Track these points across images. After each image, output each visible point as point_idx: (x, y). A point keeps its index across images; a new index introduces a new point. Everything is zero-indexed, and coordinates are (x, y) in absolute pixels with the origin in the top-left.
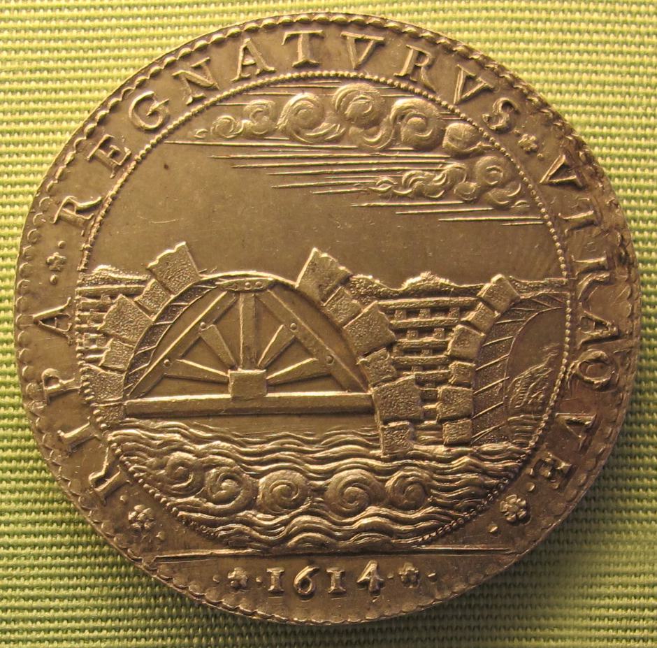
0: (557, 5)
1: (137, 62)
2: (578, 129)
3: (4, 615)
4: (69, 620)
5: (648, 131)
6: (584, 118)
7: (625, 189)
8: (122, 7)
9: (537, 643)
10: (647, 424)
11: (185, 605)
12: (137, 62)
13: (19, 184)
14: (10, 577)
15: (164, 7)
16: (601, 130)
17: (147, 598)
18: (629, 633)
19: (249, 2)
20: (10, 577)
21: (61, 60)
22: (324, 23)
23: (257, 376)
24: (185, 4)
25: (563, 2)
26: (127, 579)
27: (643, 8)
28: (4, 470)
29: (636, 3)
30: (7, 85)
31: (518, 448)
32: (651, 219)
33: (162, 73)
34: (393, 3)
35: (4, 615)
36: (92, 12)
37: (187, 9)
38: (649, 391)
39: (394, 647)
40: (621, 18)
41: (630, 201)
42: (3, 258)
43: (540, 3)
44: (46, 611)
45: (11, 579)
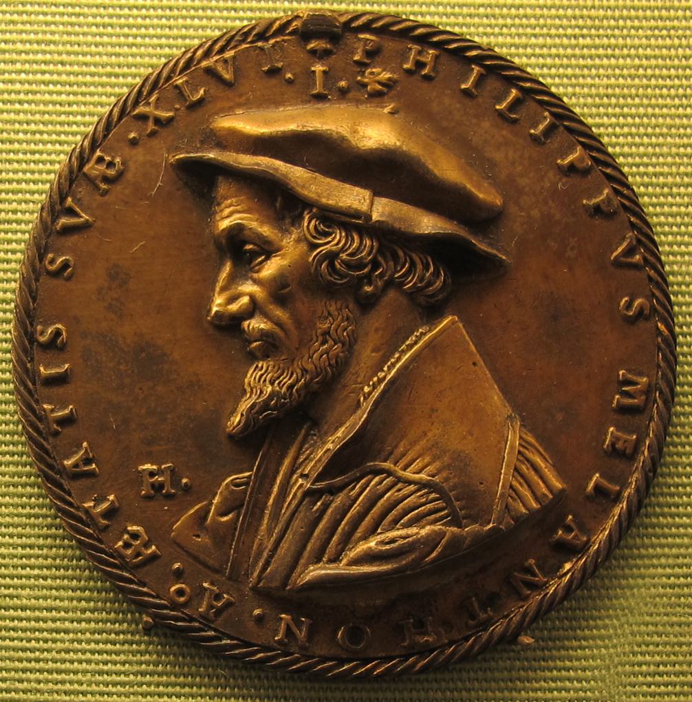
3: (3, 418)
5: (685, 121)
7: (650, 196)
8: (113, 7)
9: (9, 695)
10: (683, 446)
12: (229, 23)
16: (508, 51)
17: (158, 655)
21: (73, 73)
22: (384, 31)
23: (386, 573)
24: (36, 3)
25: (292, 2)
29: (409, 3)
30: (7, 76)
35: (3, 418)
37: (61, 9)
38: (684, 414)
41: (655, 208)
42: (5, 291)
43: (245, 2)
44: (53, 642)
45: (16, 548)
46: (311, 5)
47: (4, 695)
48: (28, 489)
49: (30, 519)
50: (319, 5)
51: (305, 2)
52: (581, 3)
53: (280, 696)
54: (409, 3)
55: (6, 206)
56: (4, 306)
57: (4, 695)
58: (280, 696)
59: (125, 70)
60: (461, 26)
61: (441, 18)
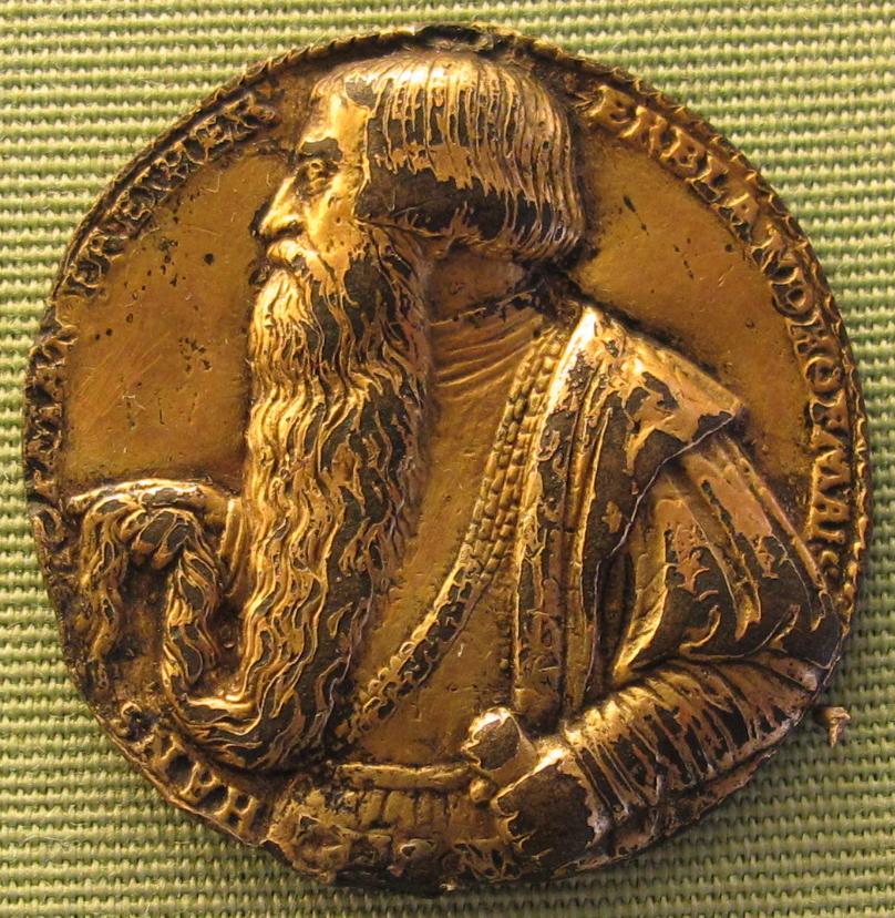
0: (860, 9)
2: (793, 207)
6: (801, 189)
11: (249, 859)
13: (46, 880)
14: (15, 137)
15: (242, 11)
18: (82, 73)
19: (432, 5)
20: (15, 137)
24: (250, 7)
26: (177, 848)
27: (713, 14)
29: (700, 6)
31: (171, 149)
32: (886, 337)
33: (466, 256)
34: (796, 5)
36: (133, 19)
37: (221, 17)
39: (514, 917)
40: (852, 28)
47: (4, 907)
48: (59, 703)
49: (22, 574)
50: (441, 10)
51: (460, 2)
52: (589, 4)
53: (384, 907)
54: (700, 6)
55: (11, 235)
56: (8, 377)
57: (4, 907)
58: (384, 907)
59: (869, 276)
60: (567, 33)
61: (172, 15)
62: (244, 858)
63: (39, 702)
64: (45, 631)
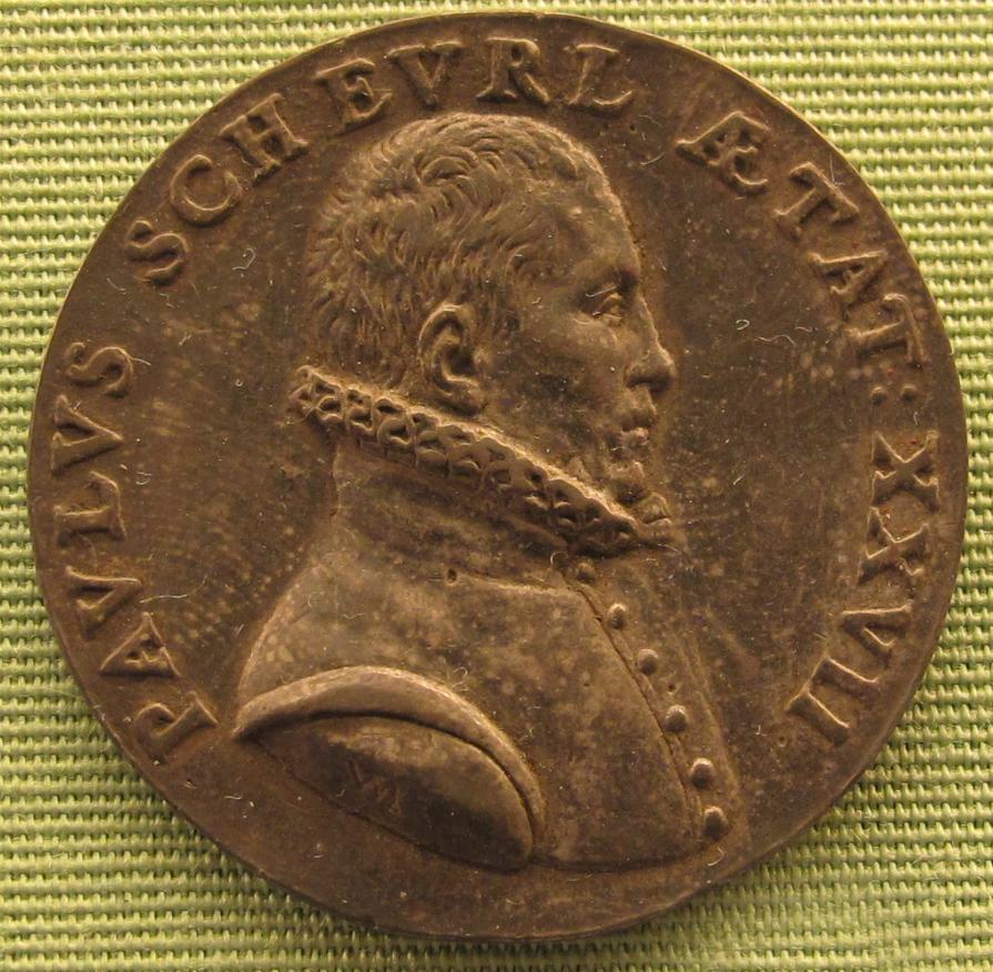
1: (217, 87)
4: (29, 254)
12: (217, 87)
28: (8, 737)
34: (211, 8)
43: (432, 4)
46: (402, 9)
62: (377, 948)
63: (65, 723)
64: (28, 588)
